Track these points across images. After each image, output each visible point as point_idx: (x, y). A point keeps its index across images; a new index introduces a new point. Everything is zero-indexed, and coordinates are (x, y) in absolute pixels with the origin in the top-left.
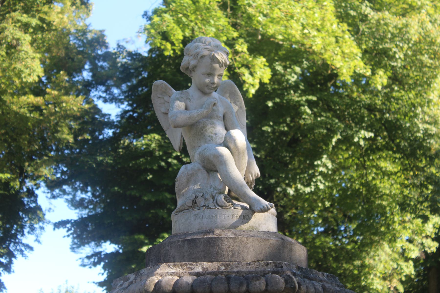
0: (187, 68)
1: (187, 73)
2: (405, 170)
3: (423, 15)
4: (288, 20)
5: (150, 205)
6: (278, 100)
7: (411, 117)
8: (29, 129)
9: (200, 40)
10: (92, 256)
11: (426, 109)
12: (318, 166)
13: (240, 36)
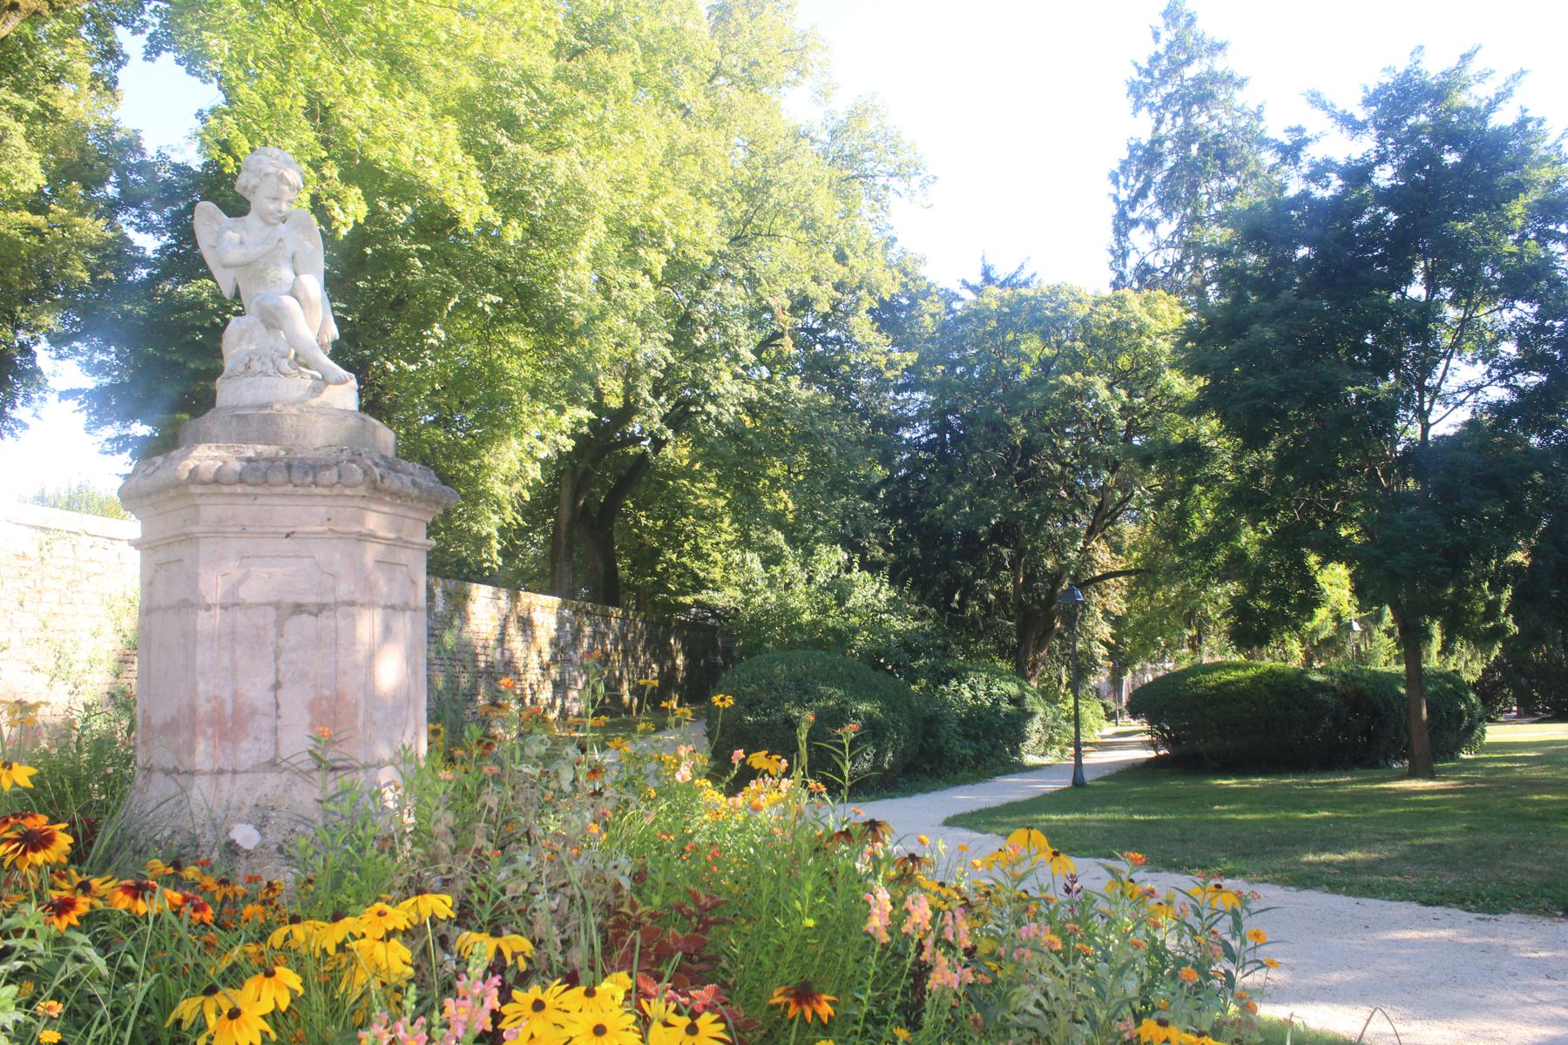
2: (540, 347)
3: (573, 156)
11: (569, 272)
13: (331, 157)
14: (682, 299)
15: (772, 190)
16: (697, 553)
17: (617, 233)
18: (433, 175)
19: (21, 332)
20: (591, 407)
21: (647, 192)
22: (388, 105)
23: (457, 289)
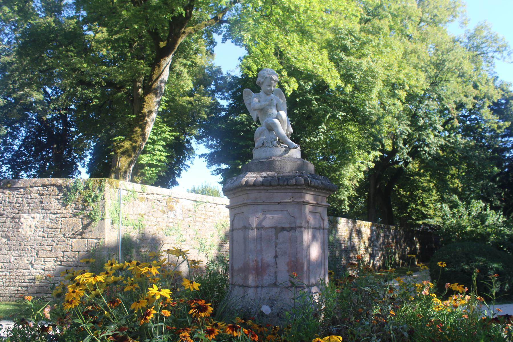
0: (259, 83)
2: (360, 130)
3: (369, 58)
4: (306, 61)
6: (301, 98)
7: (363, 106)
8: (187, 112)
9: (265, 70)
11: (370, 102)
12: (320, 128)
15: (446, 63)
16: (423, 204)
17: (387, 86)
20: (380, 151)
21: (397, 69)
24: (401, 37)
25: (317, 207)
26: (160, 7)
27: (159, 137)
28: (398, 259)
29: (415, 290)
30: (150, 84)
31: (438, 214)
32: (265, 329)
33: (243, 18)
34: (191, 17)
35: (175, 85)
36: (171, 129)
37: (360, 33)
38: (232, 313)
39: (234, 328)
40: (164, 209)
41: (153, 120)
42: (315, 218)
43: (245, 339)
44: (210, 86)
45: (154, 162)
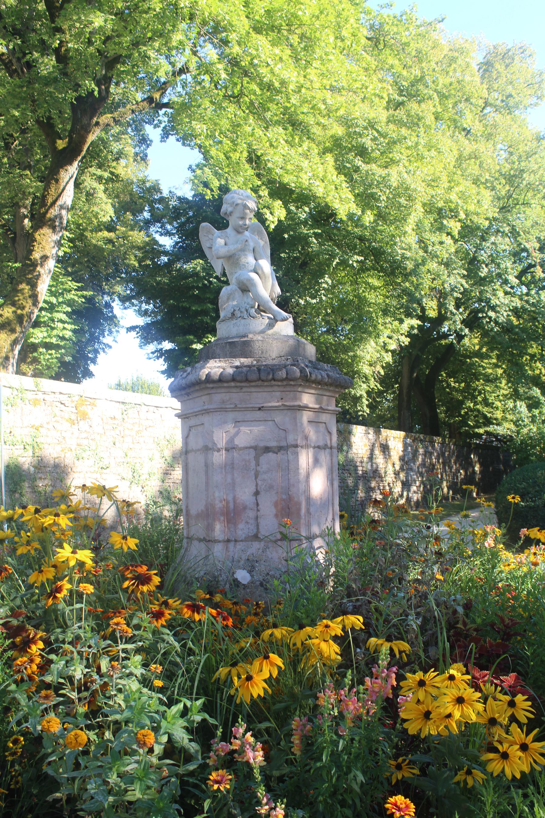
0: (226, 214)
1: (226, 217)
2: (386, 285)
3: (401, 168)
5: (197, 313)
6: (292, 233)
8: (105, 257)
10: (156, 351)
11: (402, 238)
12: (321, 283)
14: (469, 247)
15: (524, 175)
16: (486, 403)
17: (430, 212)
18: (319, 190)
19: (105, 296)
20: (419, 318)
21: (446, 185)
22: (293, 152)
23: (338, 254)
24: (454, 132)
25: (320, 414)
26: (55, 80)
27: (61, 300)
28: (445, 490)
29: (473, 540)
30: (43, 210)
31: (510, 417)
32: (243, 607)
33: (196, 100)
34: (108, 97)
35: (85, 213)
36: (79, 285)
37: (387, 125)
38: (190, 584)
39: (195, 608)
40: (73, 417)
41: (50, 271)
42: (317, 432)
43: (213, 623)
44: (142, 212)
45: (54, 341)
